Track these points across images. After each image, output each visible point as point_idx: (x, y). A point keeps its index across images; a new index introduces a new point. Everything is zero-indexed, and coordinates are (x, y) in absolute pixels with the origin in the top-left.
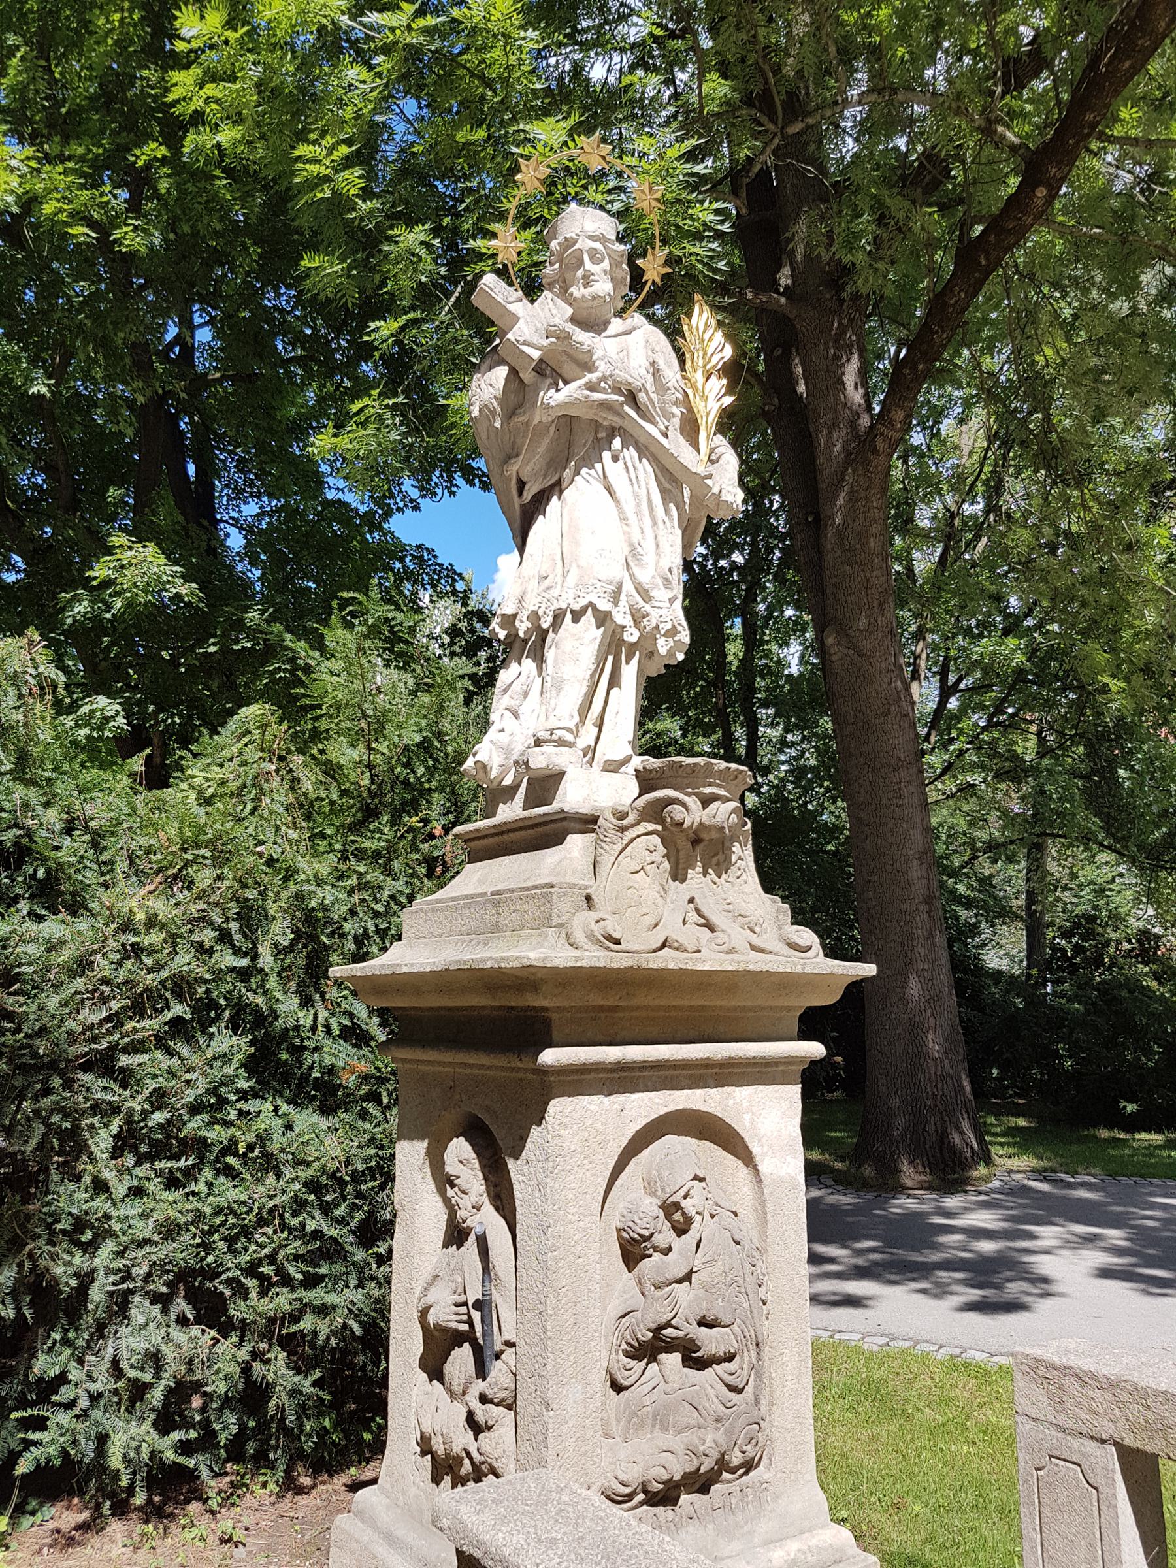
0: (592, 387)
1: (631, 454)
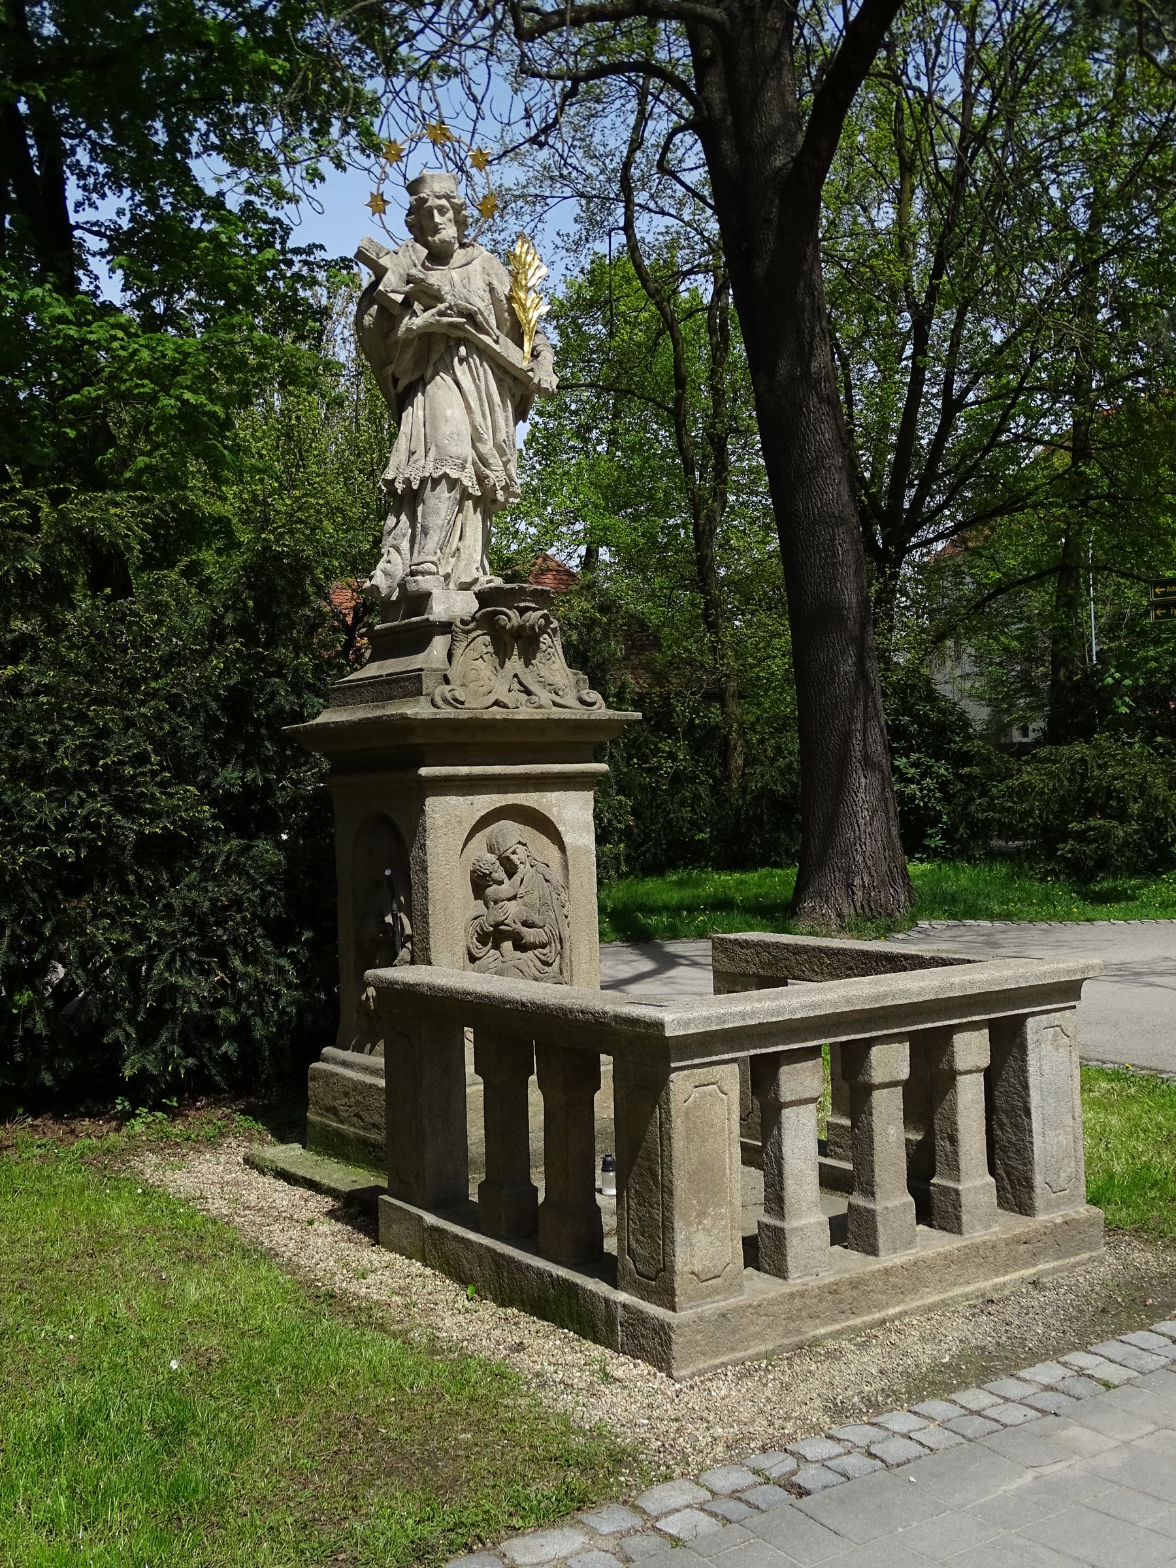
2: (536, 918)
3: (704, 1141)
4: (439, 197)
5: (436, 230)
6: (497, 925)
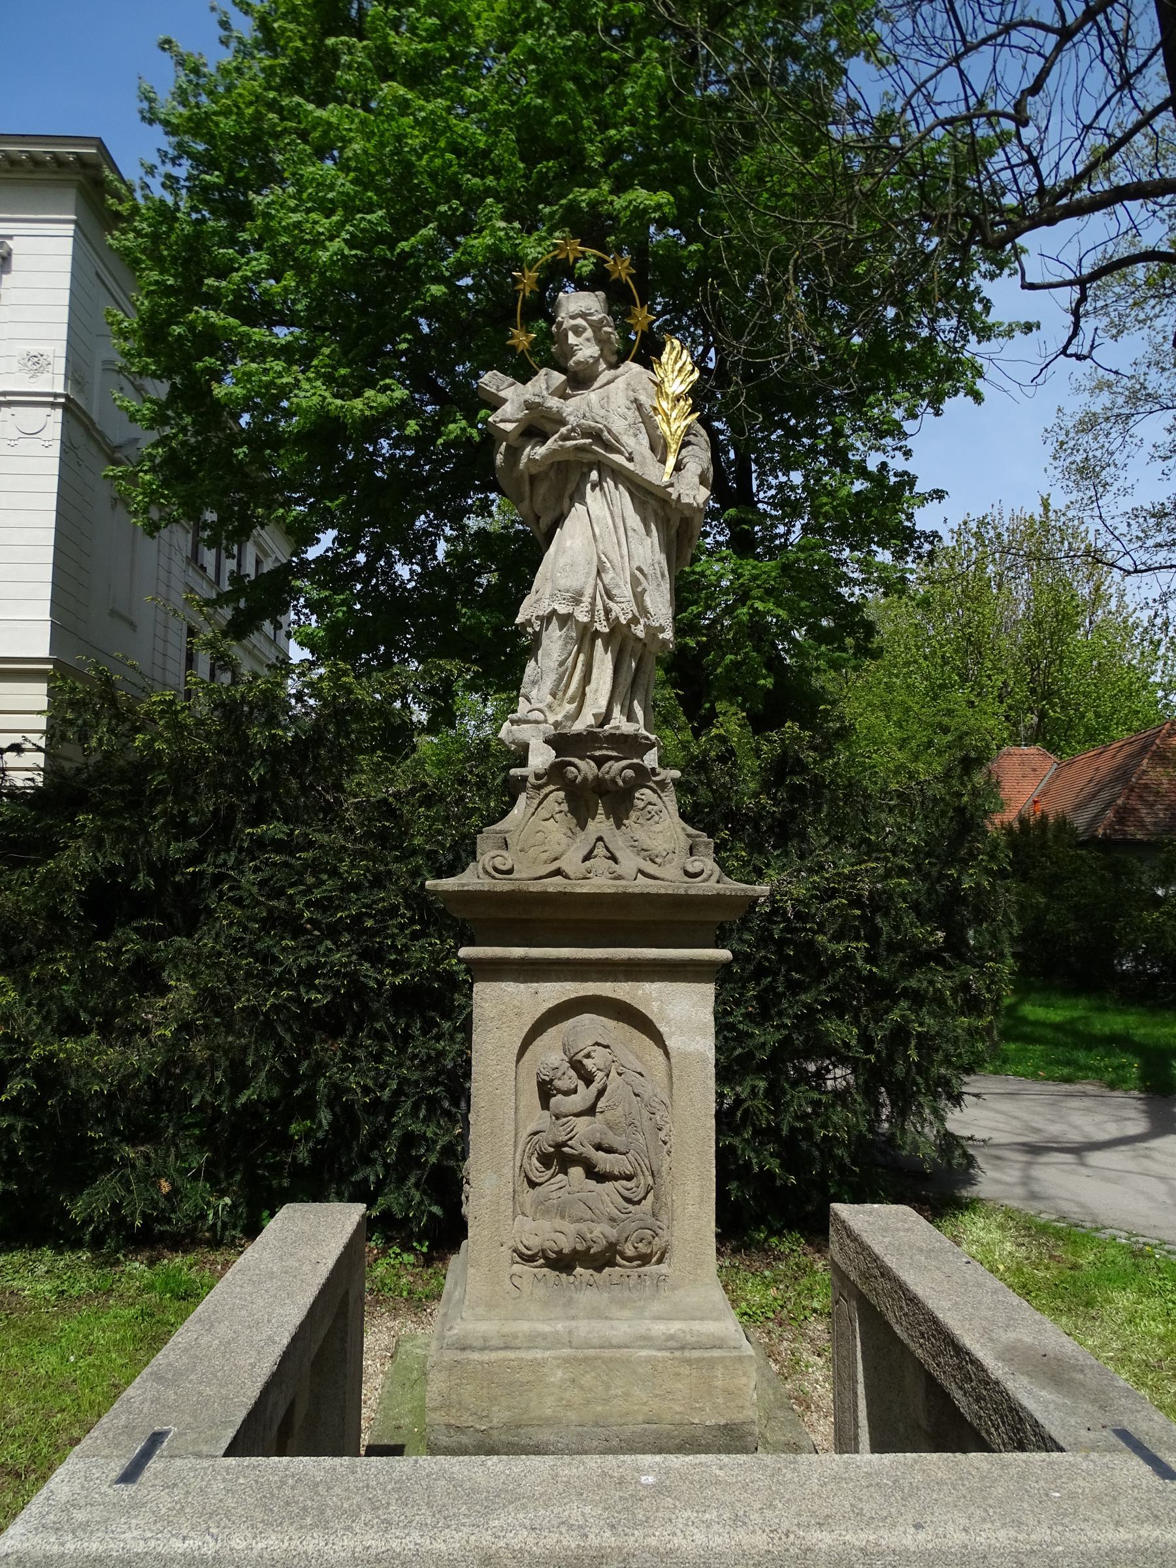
0: (565, 438)
1: (609, 484)
4: (573, 317)
5: (571, 351)
6: (559, 1146)
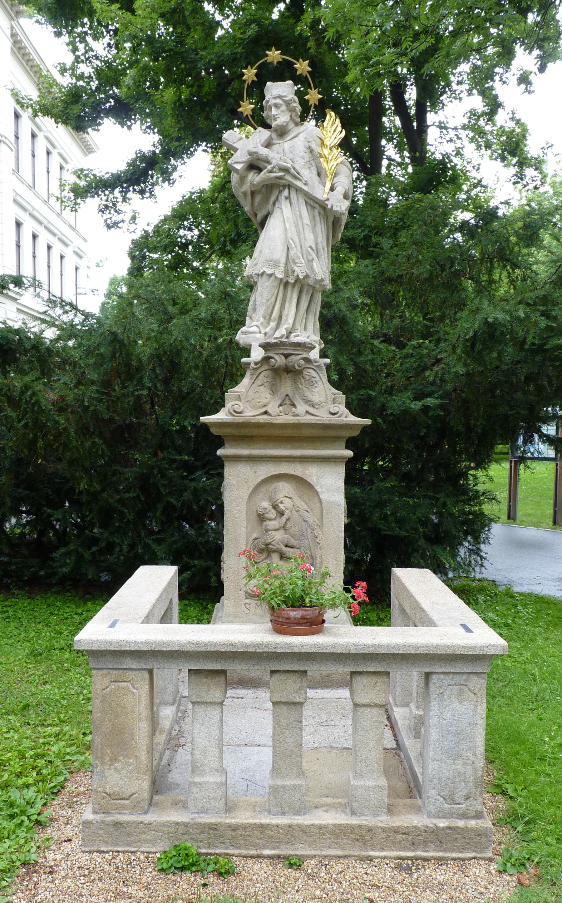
2: (293, 542)
3: (117, 716)
4: (275, 98)
